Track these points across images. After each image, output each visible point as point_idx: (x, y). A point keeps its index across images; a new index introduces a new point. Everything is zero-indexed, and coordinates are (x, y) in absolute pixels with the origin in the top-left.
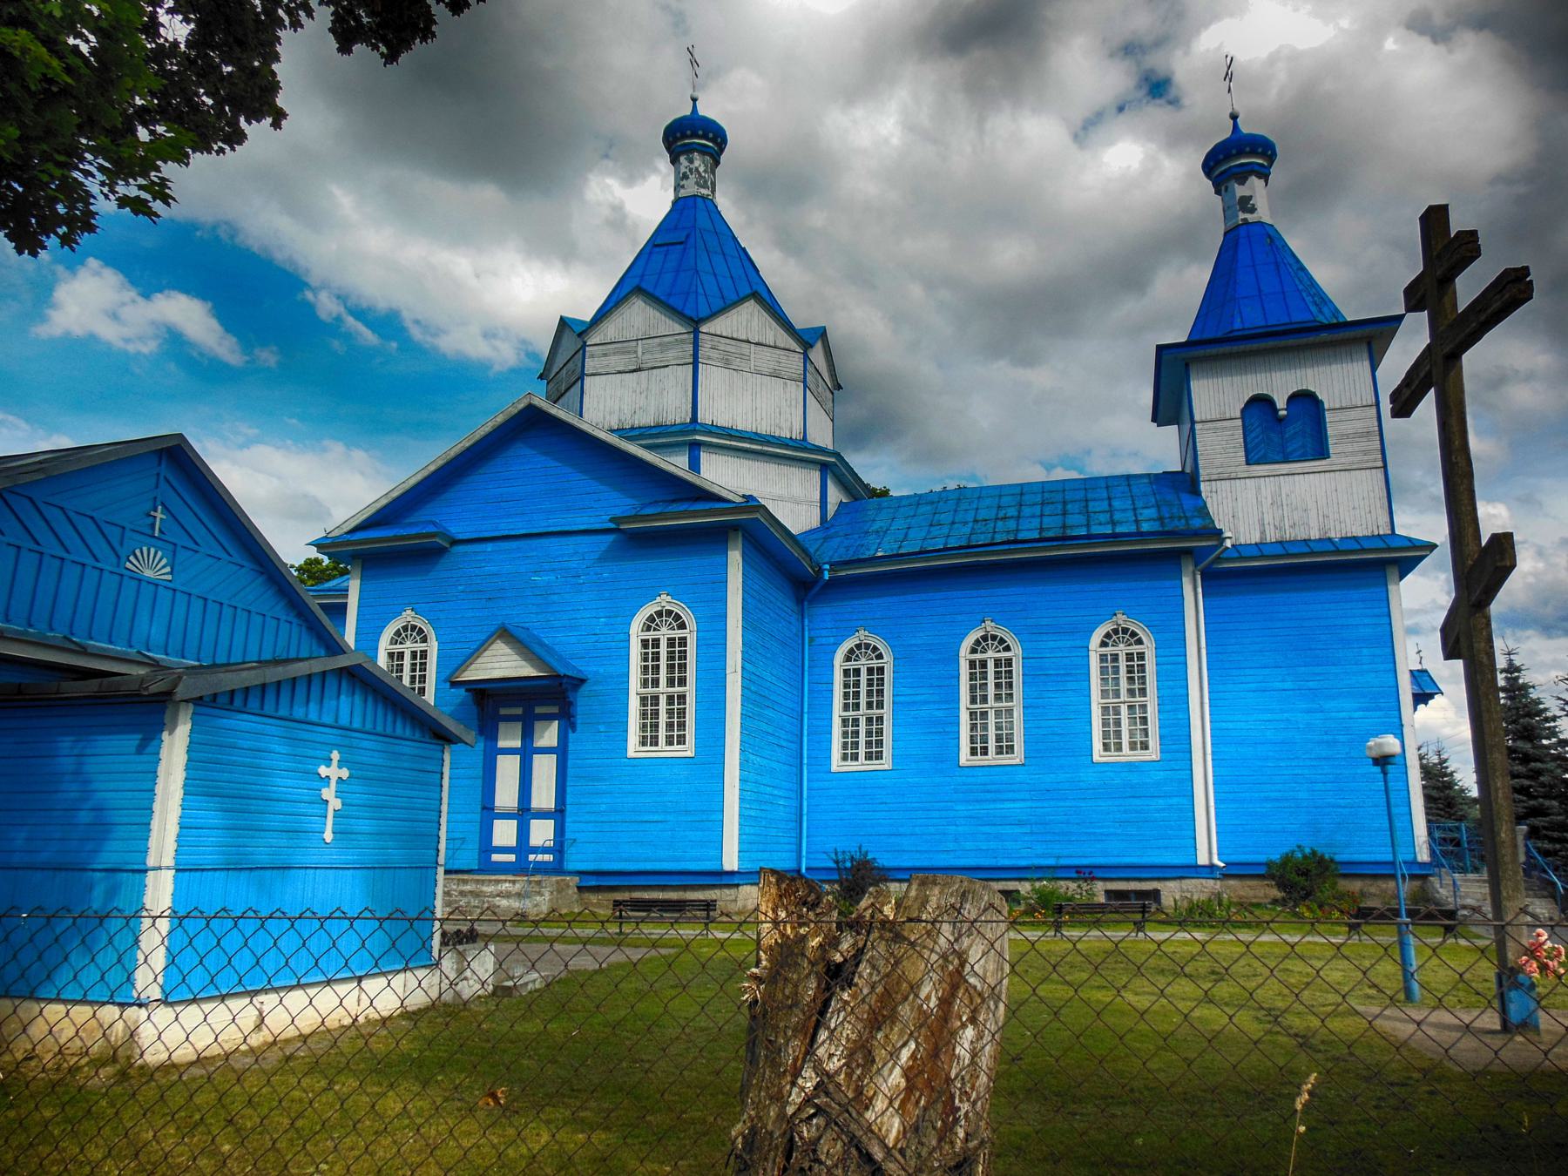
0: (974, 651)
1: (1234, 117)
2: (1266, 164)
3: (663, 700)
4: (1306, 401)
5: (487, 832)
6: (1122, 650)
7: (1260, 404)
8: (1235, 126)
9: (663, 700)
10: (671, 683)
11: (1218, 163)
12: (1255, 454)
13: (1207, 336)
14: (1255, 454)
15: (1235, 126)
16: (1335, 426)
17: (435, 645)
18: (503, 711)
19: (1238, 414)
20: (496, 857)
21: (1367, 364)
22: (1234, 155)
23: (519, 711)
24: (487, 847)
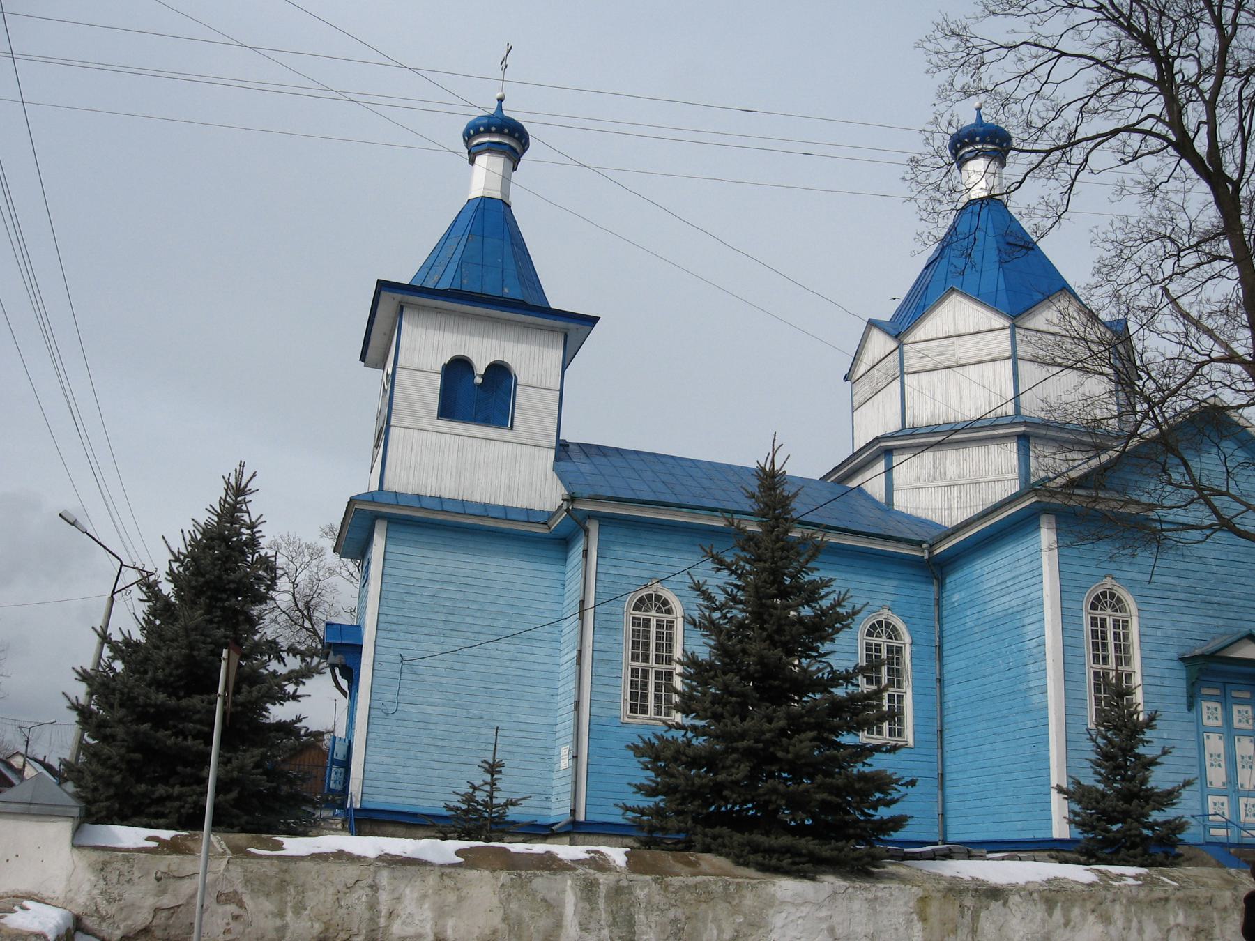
0: (869, 634)
1: (501, 100)
2: (518, 150)
3: (652, 675)
4: (500, 373)
6: (653, 615)
7: (457, 368)
8: (500, 108)
9: (652, 675)
10: (659, 660)
11: (478, 133)
12: (447, 410)
13: (430, 284)
14: (447, 410)
15: (500, 108)
16: (523, 398)
17: (907, 639)
19: (440, 369)
21: (559, 353)
22: (482, 133)
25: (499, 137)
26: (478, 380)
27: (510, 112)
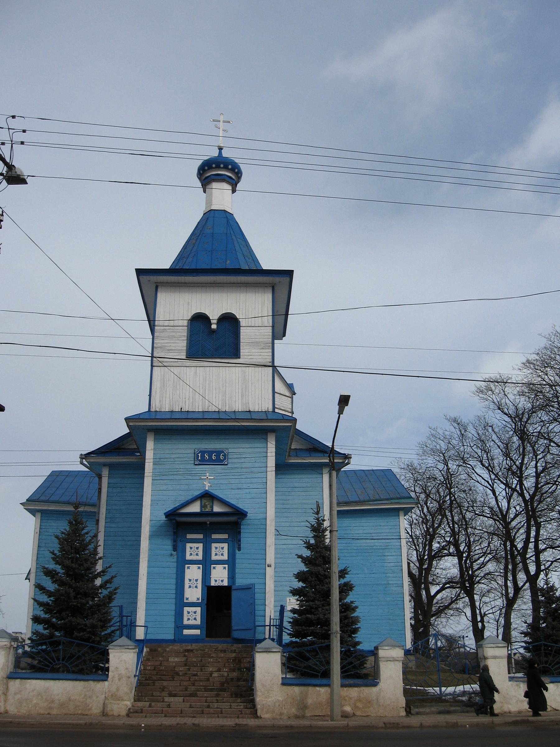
5: (179, 615)
16: (245, 333)
18: (189, 536)
20: (186, 632)
23: (201, 536)
24: (179, 626)
25: (232, 173)
26: (214, 327)
27: (226, 154)
